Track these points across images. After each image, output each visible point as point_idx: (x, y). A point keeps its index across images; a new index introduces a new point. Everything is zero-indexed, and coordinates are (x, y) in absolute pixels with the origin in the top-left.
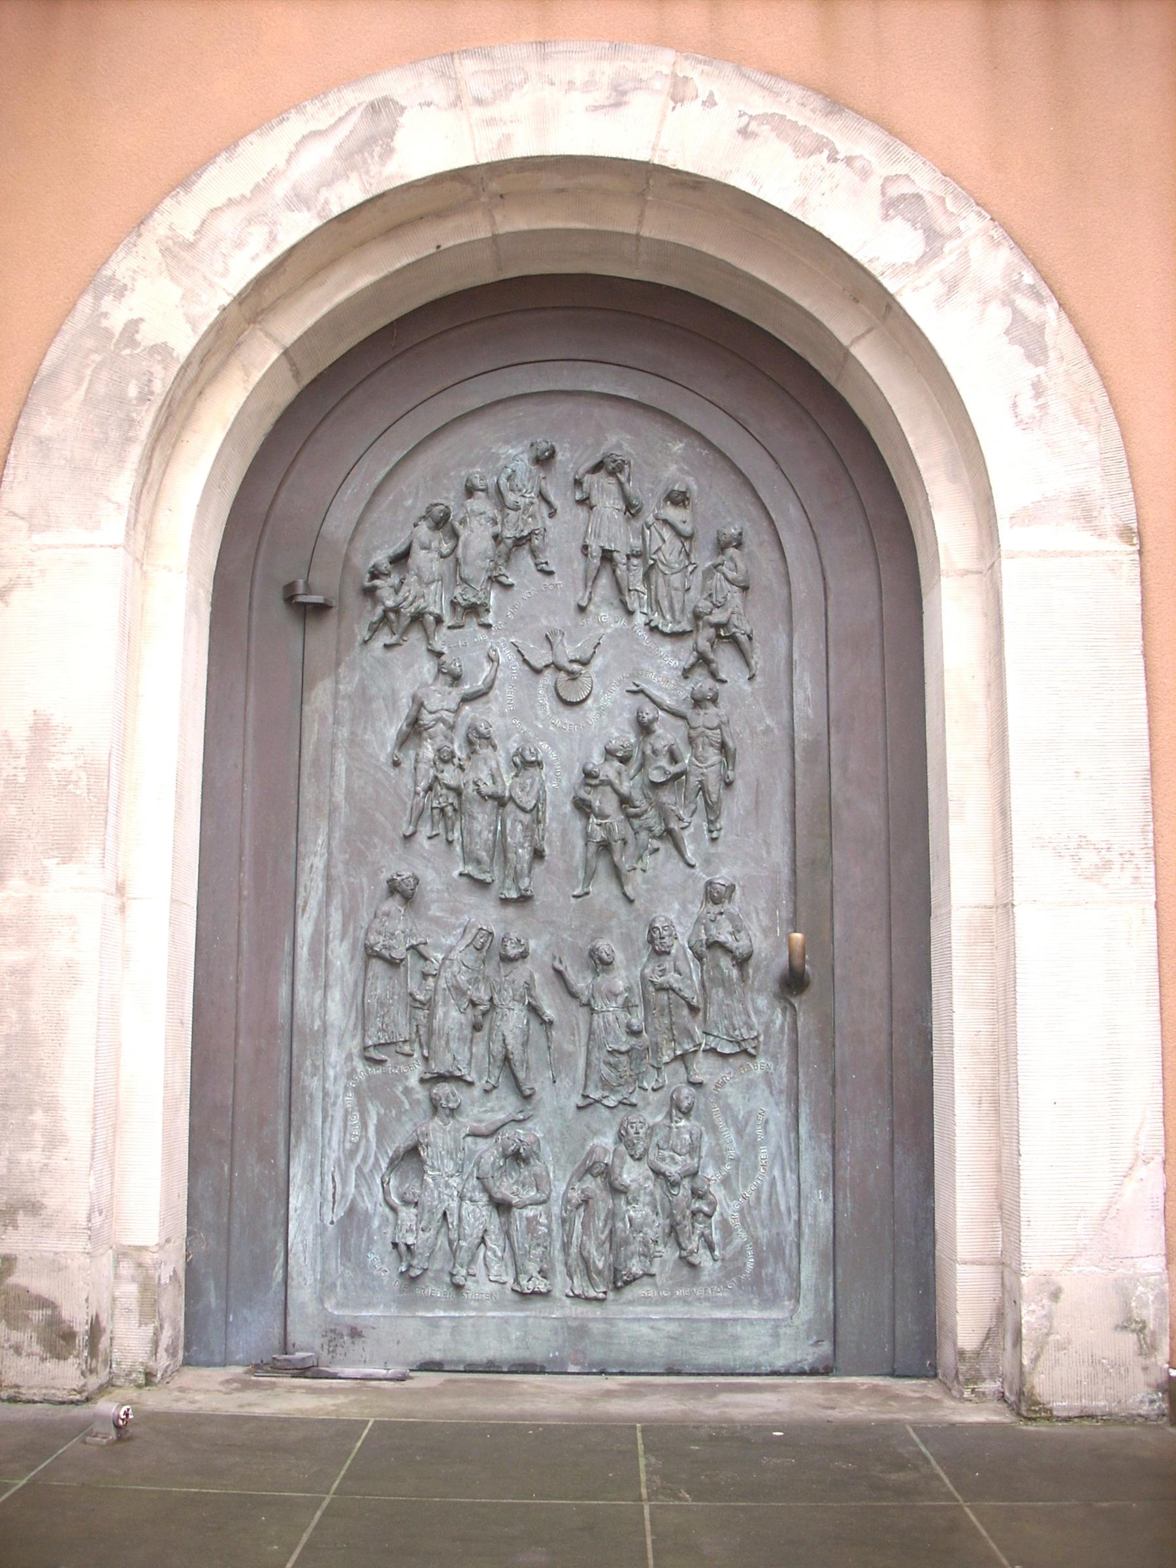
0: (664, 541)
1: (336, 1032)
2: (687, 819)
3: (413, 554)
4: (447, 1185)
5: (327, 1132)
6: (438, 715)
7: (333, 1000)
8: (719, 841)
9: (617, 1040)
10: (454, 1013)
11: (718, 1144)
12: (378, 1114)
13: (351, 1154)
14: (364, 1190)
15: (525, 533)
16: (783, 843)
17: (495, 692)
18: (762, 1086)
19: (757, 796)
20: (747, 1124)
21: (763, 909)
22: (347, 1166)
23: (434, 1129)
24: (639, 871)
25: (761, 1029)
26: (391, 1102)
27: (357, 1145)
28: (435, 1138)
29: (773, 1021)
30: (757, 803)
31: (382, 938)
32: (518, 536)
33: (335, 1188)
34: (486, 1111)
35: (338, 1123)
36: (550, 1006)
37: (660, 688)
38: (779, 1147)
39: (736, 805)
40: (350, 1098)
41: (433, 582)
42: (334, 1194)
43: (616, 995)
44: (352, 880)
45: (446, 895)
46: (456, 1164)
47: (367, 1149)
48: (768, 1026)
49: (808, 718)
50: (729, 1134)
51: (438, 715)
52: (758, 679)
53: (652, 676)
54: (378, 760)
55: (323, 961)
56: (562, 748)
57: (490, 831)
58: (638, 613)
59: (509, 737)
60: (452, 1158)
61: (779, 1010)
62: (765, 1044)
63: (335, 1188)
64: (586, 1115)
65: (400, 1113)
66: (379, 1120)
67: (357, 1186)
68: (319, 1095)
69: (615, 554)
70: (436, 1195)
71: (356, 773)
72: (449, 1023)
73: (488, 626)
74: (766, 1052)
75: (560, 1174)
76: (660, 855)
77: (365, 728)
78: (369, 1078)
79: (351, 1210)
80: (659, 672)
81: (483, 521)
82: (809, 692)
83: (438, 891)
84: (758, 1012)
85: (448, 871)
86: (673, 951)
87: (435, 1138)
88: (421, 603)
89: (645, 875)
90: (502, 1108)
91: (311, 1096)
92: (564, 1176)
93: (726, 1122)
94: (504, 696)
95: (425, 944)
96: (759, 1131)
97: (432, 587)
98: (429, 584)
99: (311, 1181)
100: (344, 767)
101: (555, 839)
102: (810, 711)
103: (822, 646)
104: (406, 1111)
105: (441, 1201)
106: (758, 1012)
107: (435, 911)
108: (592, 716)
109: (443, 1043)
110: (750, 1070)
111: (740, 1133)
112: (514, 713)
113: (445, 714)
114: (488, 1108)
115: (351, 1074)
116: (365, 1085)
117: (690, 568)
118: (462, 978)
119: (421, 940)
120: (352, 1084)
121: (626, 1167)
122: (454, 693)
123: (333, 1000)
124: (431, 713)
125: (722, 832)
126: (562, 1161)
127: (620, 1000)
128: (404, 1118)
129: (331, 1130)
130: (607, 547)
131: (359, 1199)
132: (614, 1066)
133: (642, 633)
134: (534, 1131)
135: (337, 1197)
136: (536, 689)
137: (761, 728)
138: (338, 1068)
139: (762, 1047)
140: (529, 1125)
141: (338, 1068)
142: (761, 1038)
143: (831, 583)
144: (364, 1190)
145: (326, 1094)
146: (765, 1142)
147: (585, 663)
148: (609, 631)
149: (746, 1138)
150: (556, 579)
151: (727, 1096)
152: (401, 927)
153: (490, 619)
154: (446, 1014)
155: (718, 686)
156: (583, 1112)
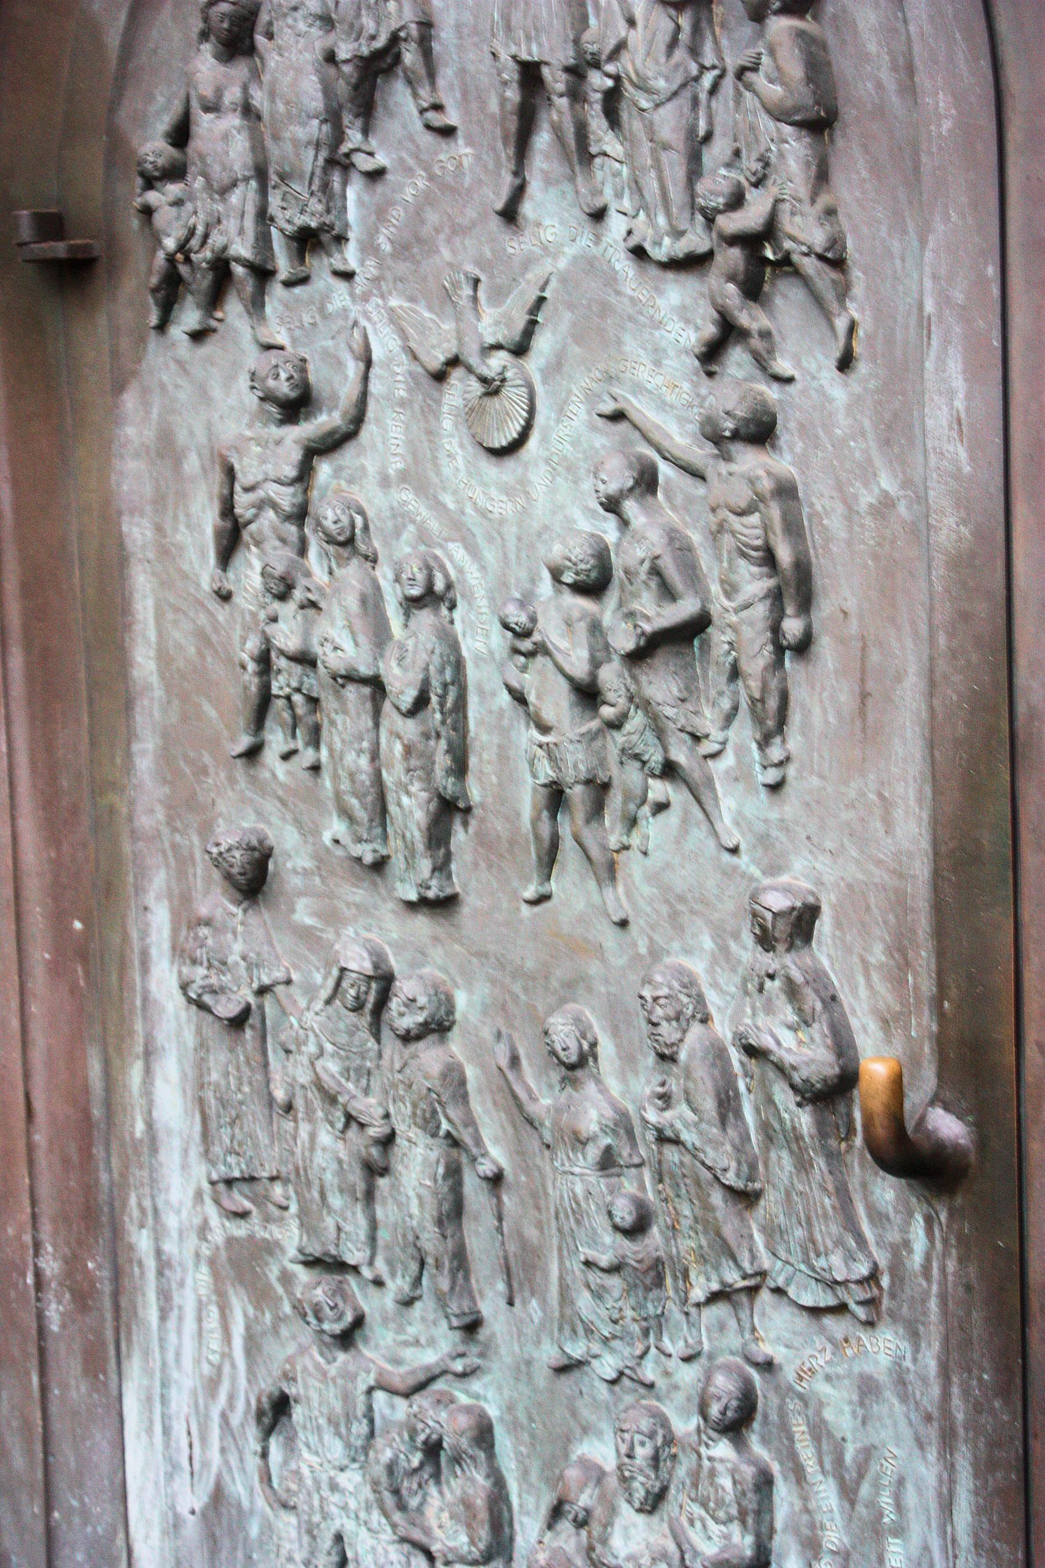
0: (631, 22)
1: (176, 1142)
2: (716, 734)
3: (195, 129)
4: (334, 1487)
5: (172, 1338)
6: (260, 493)
7: (166, 1080)
8: (787, 789)
9: (594, 1240)
10: (325, 1138)
11: (807, 1510)
12: (246, 1315)
13: (212, 1385)
14: (233, 1460)
15: (380, 43)
16: (920, 801)
17: (369, 431)
18: (889, 1394)
19: (863, 680)
20: (861, 1476)
21: (881, 967)
22: (207, 1408)
23: (305, 1369)
24: (634, 854)
25: (883, 1259)
26: (261, 1296)
27: (219, 1369)
28: (306, 1387)
29: (907, 1244)
30: (864, 696)
31: (201, 971)
32: (365, 51)
33: (191, 1446)
34: (406, 1344)
35: (190, 1325)
36: (496, 1141)
37: (663, 406)
38: (926, 1548)
39: (819, 695)
40: (204, 1275)
41: (234, 184)
42: (191, 1459)
43: (584, 1143)
44: (178, 838)
45: (317, 880)
46: (348, 1445)
47: (234, 1379)
48: (899, 1250)
49: (957, 475)
50: (827, 1494)
51: (260, 493)
52: (862, 368)
53: (644, 374)
54: (198, 586)
55: (138, 1003)
56: (490, 555)
57: (360, 752)
58: (612, 213)
59: (397, 533)
60: (338, 1434)
61: (919, 1218)
62: (893, 1296)
63: (191, 1446)
64: (566, 1383)
65: (279, 1320)
66: (248, 1328)
67: (223, 1450)
68: (151, 1264)
69: (545, 71)
70: (316, 1502)
71: (170, 616)
72: (319, 1159)
73: (348, 276)
74: (893, 1315)
75: (530, 1501)
76: (672, 818)
77: (175, 518)
78: (230, 1241)
79: (218, 1496)
80: (658, 363)
81: (302, 26)
82: (959, 404)
83: (306, 873)
84: (877, 1217)
85: (316, 832)
86: (683, 1056)
87: (306, 1387)
88: (217, 240)
89: (648, 862)
90: (432, 1342)
91: (140, 1264)
92: (537, 1507)
93: (821, 1463)
94: (386, 435)
95: (289, 982)
96: (886, 1500)
97: (235, 198)
98: (224, 191)
99: (150, 1431)
100: (150, 603)
101: (488, 769)
102: (963, 454)
103: (992, 271)
104: (287, 1316)
105: (326, 1516)
106: (877, 1217)
107: (303, 914)
108: (539, 478)
109: (316, 1195)
110: (862, 1352)
111: (848, 1493)
112: (404, 477)
113: (272, 490)
114: (412, 1340)
115: (203, 1230)
116: (223, 1255)
117: (707, 80)
118: (330, 1067)
119: (279, 975)
120: (206, 1251)
121: (619, 1523)
122: (288, 442)
123: (166, 1080)
124: (247, 490)
125: (791, 771)
126: (534, 1477)
127: (593, 1153)
128: (284, 1331)
129: (179, 1332)
130: (525, 56)
131: (227, 1478)
132: (598, 1294)
133: (624, 265)
134: (490, 1396)
135: (197, 1466)
136: (437, 416)
137: (867, 499)
138: (184, 1214)
139: (886, 1302)
140: (476, 1385)
141: (184, 1214)
142: (885, 1281)
143: (1015, 80)
144: (233, 1460)
145: (163, 1265)
146: (899, 1531)
147: (520, 350)
148: (562, 264)
149: (861, 1509)
150: (462, 148)
151: (821, 1404)
152: (238, 947)
153: (351, 256)
154: (313, 1136)
155: (772, 393)
156: (563, 1378)
